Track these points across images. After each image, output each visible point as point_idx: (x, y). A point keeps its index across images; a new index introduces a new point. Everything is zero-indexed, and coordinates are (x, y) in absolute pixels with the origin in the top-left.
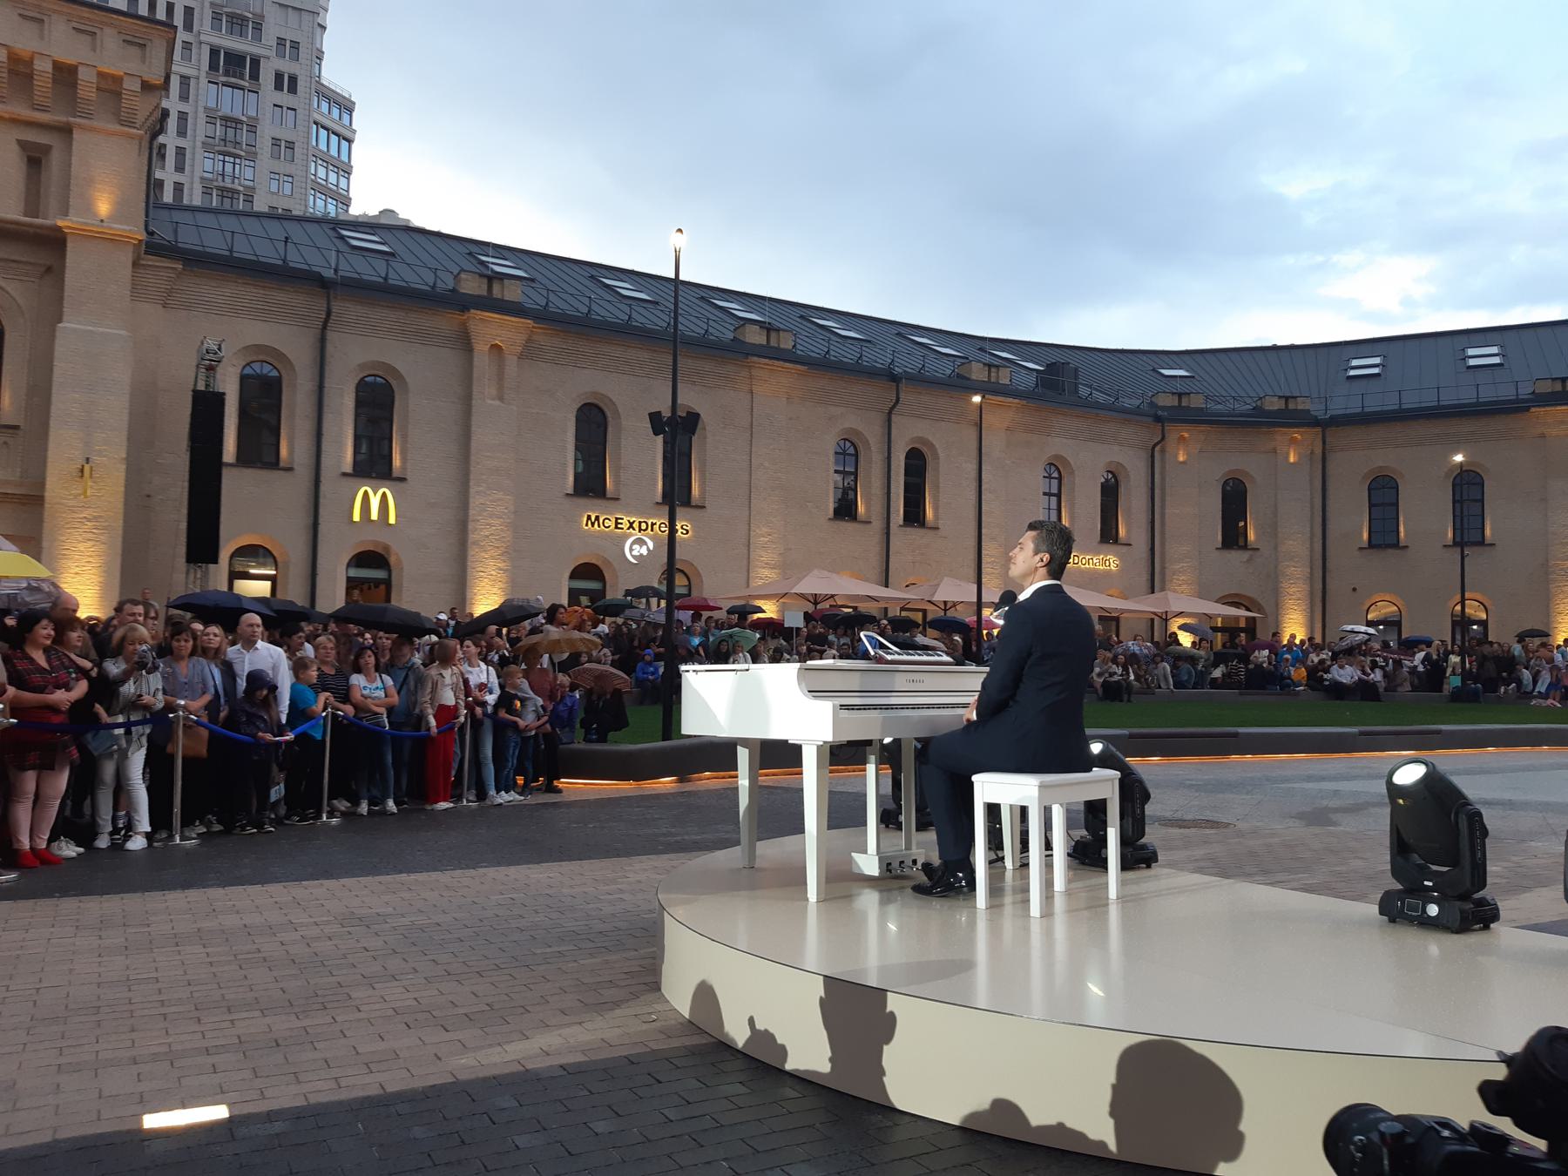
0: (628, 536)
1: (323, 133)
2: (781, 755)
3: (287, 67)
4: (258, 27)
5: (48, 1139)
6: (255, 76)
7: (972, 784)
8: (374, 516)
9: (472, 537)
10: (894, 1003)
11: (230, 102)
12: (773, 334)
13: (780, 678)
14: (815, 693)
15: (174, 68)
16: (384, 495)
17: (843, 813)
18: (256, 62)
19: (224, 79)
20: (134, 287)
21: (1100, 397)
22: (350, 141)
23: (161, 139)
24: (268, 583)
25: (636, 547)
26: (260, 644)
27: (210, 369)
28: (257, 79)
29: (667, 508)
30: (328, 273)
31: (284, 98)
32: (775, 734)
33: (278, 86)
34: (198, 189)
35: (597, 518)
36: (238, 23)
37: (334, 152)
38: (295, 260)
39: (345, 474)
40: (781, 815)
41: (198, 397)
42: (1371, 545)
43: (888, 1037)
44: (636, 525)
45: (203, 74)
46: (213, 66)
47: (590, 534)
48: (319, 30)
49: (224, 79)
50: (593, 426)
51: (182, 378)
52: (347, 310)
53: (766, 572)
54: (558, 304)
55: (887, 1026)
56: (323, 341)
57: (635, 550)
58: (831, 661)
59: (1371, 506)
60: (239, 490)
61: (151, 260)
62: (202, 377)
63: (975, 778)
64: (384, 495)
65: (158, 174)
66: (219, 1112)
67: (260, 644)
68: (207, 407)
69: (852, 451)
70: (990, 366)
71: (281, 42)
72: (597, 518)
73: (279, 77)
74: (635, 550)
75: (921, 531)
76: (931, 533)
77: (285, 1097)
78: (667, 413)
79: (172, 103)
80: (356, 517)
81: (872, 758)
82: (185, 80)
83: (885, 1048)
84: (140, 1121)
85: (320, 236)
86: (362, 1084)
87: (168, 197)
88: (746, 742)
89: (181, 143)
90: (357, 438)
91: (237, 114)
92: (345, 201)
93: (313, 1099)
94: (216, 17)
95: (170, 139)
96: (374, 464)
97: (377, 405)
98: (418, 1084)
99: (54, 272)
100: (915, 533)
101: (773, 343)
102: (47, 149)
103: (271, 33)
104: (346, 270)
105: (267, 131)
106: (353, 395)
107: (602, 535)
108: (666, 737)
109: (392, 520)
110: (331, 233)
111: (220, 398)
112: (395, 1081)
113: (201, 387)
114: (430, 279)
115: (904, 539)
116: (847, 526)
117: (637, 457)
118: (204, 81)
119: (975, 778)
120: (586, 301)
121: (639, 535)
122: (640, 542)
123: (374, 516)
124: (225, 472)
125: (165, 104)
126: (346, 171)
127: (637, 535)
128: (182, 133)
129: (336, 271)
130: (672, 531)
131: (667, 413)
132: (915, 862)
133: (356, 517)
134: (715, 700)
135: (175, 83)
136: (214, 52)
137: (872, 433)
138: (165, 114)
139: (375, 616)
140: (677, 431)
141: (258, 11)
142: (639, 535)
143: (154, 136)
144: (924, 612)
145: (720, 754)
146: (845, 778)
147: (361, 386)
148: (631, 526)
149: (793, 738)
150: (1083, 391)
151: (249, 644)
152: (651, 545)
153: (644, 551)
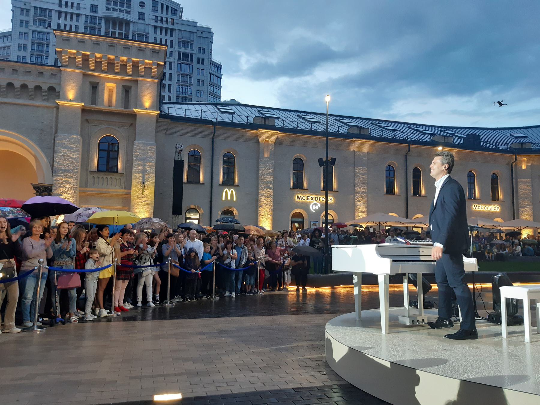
0: (310, 203)
1: (212, 76)
2: (370, 279)
3: (201, 56)
4: (192, 44)
5: (125, 401)
6: (191, 60)
7: (500, 290)
8: (229, 198)
9: (260, 204)
10: (418, 372)
11: (184, 69)
12: (362, 130)
13: (369, 250)
14: (383, 256)
15: (167, 60)
16: (232, 191)
17: (395, 300)
18: (192, 56)
19: (182, 62)
20: (156, 129)
21: (489, 146)
22: (220, 78)
23: (164, 82)
24: (197, 221)
25: (314, 206)
26: (196, 240)
27: (179, 153)
28: (192, 61)
29: (324, 192)
30: (214, 120)
31: (200, 66)
32: (368, 270)
33: (199, 63)
34: (175, 98)
35: (301, 197)
36: (186, 44)
37: (216, 82)
38: (204, 117)
39: (220, 185)
40: (372, 301)
41: (175, 162)
42: (98, 170)
43: (418, 384)
44: (314, 199)
45: (176, 61)
46: (179, 58)
47: (298, 202)
48: (210, 43)
49: (182, 62)
50: (298, 164)
51: (171, 157)
52: (220, 132)
53: (360, 214)
54: (287, 125)
55: (416, 380)
56: (213, 142)
57: (314, 208)
58: (388, 244)
59: (99, 150)
60: (188, 191)
61: (161, 120)
62: (177, 156)
63: (501, 288)
64: (232, 191)
65: (163, 94)
66: (178, 396)
67: (196, 240)
68: (178, 165)
69: (392, 169)
70: (444, 136)
71: (199, 48)
72: (301, 197)
73: (199, 59)
74: (314, 208)
75: (420, 198)
76: (203, 186)
77: (200, 392)
78: (324, 159)
79: (167, 71)
80: (224, 199)
81: (406, 281)
82: (171, 63)
83: (416, 387)
84: (153, 397)
85: (294, 116)
86: (224, 390)
87: (166, 100)
88: (356, 274)
89: (170, 83)
90: (223, 173)
91: (186, 73)
92: (220, 97)
93: (209, 394)
94: (180, 42)
95: (166, 82)
96: (229, 182)
97: (229, 162)
98: (244, 391)
99: (133, 125)
100: (417, 198)
101: (362, 133)
102: (130, 87)
103: (195, 47)
104: (220, 119)
105: (195, 77)
106: (222, 159)
107: (302, 203)
108: (326, 272)
109: (235, 199)
110: (215, 108)
111: (182, 162)
112: (236, 390)
113: (176, 159)
114: (246, 120)
115: (412, 200)
116: (390, 196)
117: (313, 174)
118: (176, 63)
119: (501, 288)
120: (296, 123)
121: (315, 202)
122: (315, 204)
123: (229, 198)
124: (184, 185)
125: (165, 71)
126: (220, 88)
127: (314, 202)
128: (170, 80)
129: (217, 119)
130: (327, 200)
131: (324, 159)
132: (423, 320)
133: (224, 199)
134: (347, 258)
135: (168, 64)
136: (179, 54)
137: (397, 163)
138: (165, 73)
139: (228, 231)
140: (327, 165)
141: (192, 39)
142: (315, 202)
143: (162, 80)
144: (422, 228)
145: (346, 278)
146: (396, 288)
147: (225, 156)
148: (312, 199)
149: (374, 272)
150: (483, 144)
151: (193, 239)
152: (319, 205)
153: (317, 208)
